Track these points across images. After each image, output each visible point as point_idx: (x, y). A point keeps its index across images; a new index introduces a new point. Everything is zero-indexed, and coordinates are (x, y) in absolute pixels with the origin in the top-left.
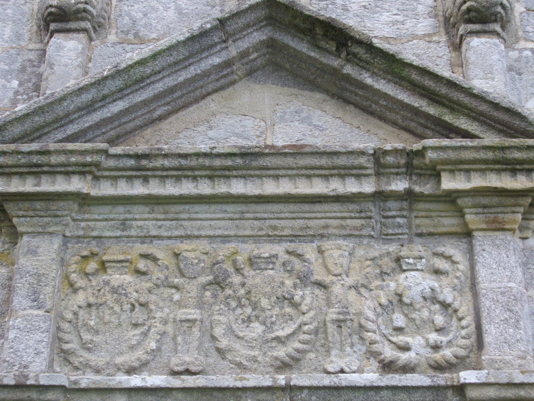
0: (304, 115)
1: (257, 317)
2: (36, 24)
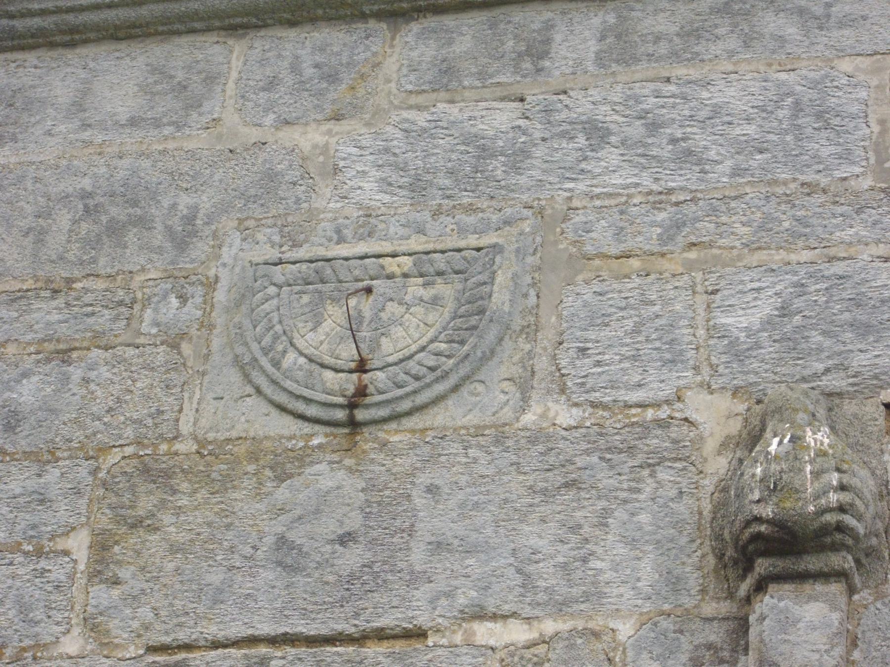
2: (713, 549)
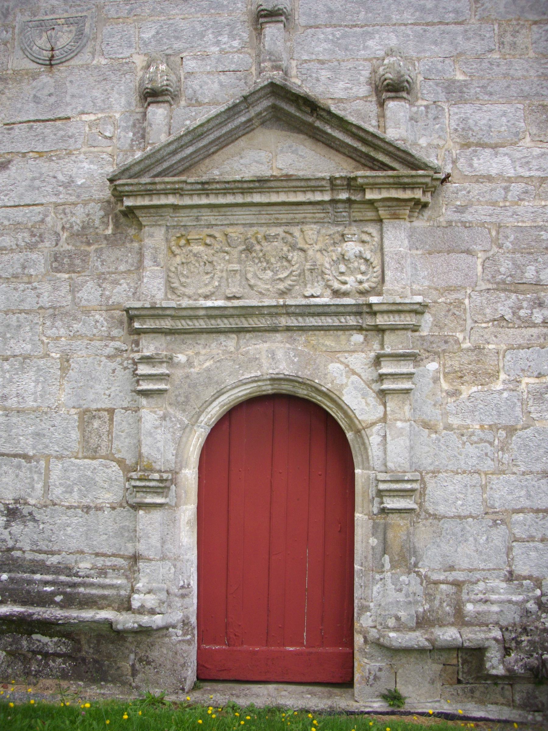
0: (293, 149)
1: (269, 268)
